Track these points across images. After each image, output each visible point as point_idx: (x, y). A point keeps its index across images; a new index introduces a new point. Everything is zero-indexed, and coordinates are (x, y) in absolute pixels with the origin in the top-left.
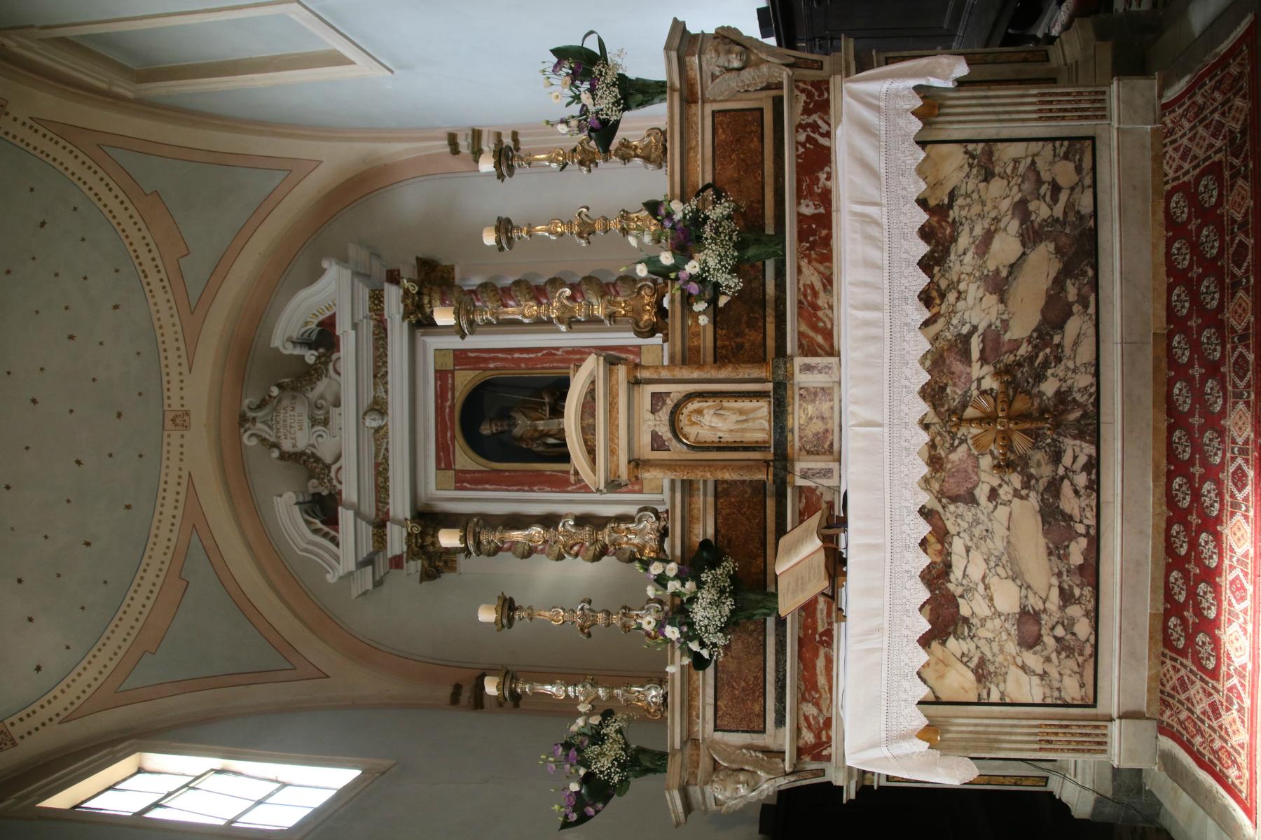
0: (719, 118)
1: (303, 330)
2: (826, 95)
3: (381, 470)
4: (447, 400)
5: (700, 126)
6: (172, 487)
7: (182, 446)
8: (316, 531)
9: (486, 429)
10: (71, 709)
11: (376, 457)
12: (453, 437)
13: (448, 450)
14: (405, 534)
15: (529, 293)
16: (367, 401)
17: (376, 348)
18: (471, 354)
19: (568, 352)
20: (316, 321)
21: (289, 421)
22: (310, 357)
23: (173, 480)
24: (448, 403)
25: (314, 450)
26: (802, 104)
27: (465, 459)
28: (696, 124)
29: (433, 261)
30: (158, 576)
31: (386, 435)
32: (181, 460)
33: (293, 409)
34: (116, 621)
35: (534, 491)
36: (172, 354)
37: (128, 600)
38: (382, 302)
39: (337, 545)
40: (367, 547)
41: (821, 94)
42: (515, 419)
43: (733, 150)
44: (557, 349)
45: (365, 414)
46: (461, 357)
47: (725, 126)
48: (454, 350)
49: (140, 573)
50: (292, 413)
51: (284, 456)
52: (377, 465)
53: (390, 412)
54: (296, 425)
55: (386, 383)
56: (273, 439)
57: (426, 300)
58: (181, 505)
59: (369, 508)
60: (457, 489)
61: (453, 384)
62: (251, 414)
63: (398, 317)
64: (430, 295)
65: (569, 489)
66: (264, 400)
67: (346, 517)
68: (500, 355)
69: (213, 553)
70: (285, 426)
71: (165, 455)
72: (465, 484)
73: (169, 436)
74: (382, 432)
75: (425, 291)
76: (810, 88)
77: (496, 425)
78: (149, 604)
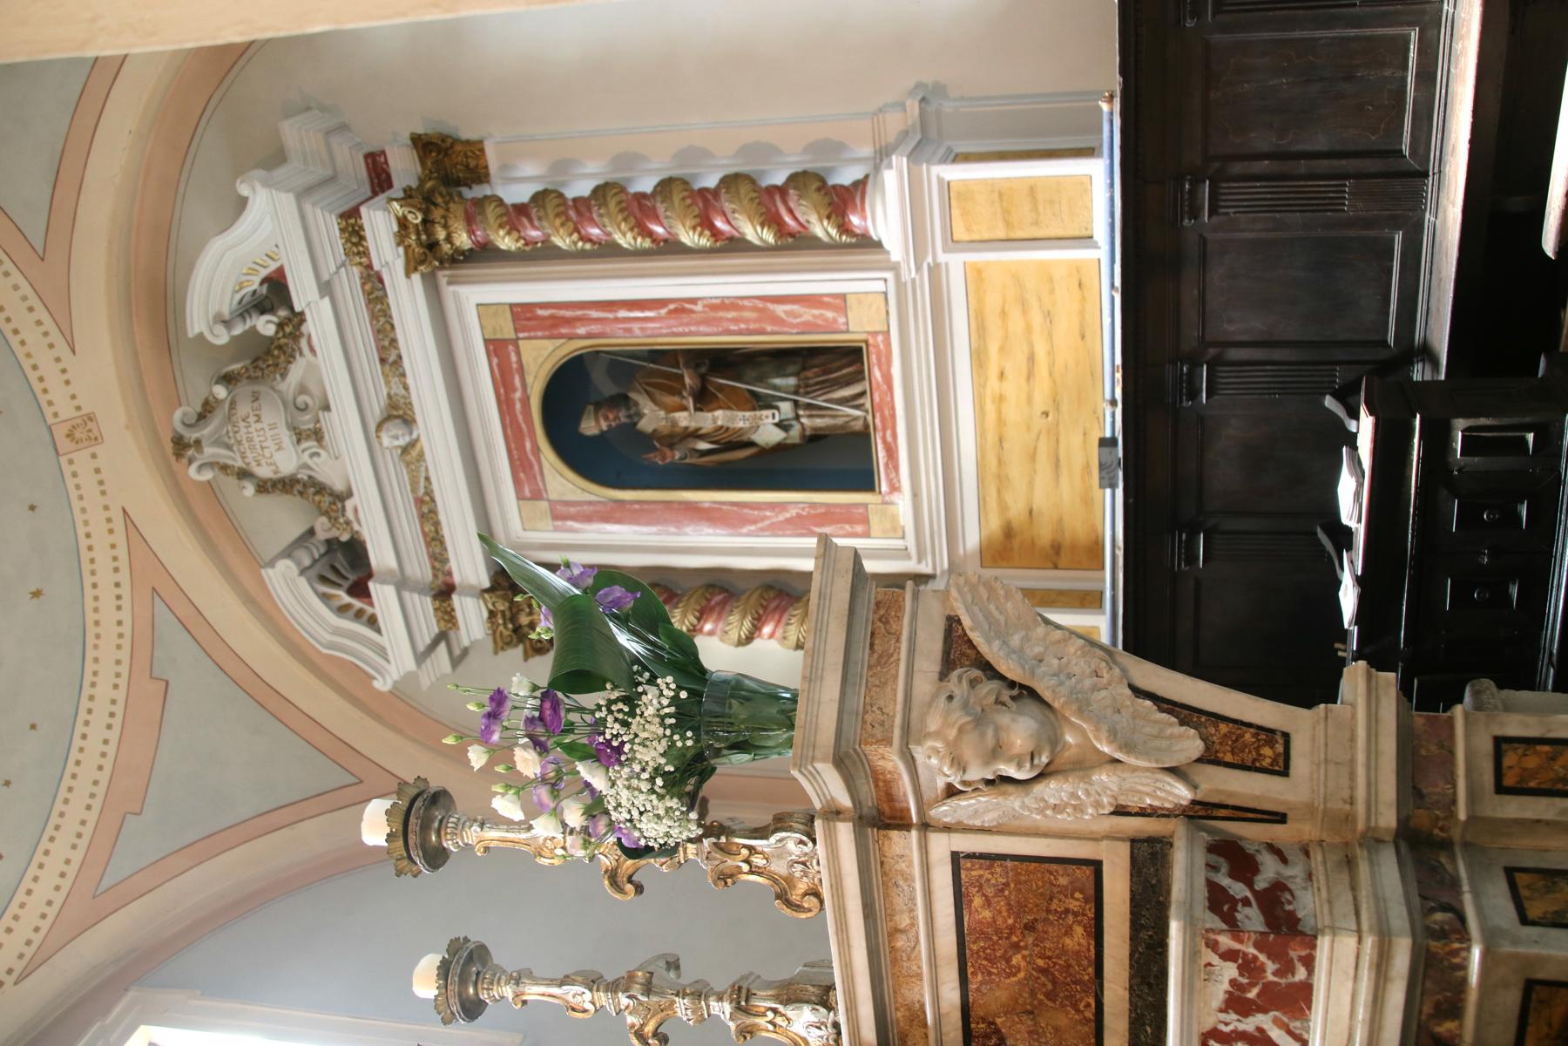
0: (971, 873)
1: (238, 297)
2: (1301, 974)
3: (427, 510)
4: (515, 390)
5: (918, 885)
6: (101, 540)
7: (98, 471)
8: (342, 610)
9: (590, 426)
10: (29, 952)
11: (414, 490)
12: (536, 450)
13: (531, 466)
14: (485, 614)
15: (625, 220)
16: (376, 410)
17: (374, 317)
18: (541, 312)
19: (713, 308)
20: (257, 280)
21: (257, 439)
22: (266, 325)
23: (98, 527)
24: (518, 395)
25: (312, 473)
26: (1226, 986)
27: (561, 481)
28: (908, 879)
29: (444, 138)
30: (116, 686)
31: (421, 456)
32: (103, 493)
33: (259, 420)
34: (67, 781)
35: (686, 534)
36: (31, 335)
37: (77, 742)
38: (362, 238)
39: (379, 631)
40: (428, 627)
41: (1287, 968)
42: (636, 404)
43: (1016, 947)
44: (694, 301)
45: (379, 427)
46: (523, 314)
47: (990, 891)
48: (512, 306)
49: (87, 690)
50: (259, 426)
51: (264, 487)
52: (419, 502)
53: (419, 418)
54: (270, 443)
55: (403, 375)
56: (239, 463)
57: (441, 234)
58: (123, 564)
59: (420, 568)
60: (556, 529)
61: (520, 361)
62: (191, 436)
63: (399, 265)
64: (446, 226)
65: (745, 530)
66: (206, 403)
67: (383, 595)
68: (594, 314)
69: (195, 626)
70: (253, 448)
71: (74, 494)
72: (570, 523)
73: (71, 462)
74: (414, 453)
75: (437, 214)
76: (1252, 950)
77: (606, 418)
78: (113, 735)
